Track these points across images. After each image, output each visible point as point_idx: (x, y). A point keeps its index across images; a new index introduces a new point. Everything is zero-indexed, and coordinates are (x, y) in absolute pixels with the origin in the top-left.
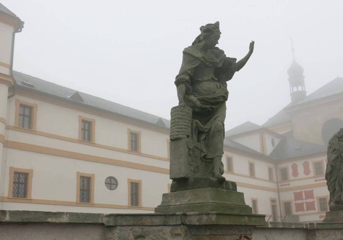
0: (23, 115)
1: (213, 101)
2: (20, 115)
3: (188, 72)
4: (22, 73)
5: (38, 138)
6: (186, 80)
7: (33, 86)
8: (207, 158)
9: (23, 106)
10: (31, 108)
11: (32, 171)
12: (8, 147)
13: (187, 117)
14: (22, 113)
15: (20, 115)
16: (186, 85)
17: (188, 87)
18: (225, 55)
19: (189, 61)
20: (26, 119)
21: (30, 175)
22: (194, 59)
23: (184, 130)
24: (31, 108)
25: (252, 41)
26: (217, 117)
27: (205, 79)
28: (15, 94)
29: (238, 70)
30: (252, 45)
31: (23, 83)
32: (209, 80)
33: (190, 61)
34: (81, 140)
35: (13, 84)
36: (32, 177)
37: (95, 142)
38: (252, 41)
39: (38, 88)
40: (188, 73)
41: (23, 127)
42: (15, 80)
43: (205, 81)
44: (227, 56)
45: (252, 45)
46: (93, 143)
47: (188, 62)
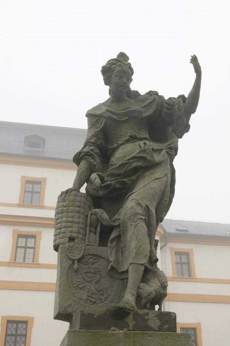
0: (181, 263)
1: (123, 171)
2: (177, 263)
3: (91, 141)
4: (184, 220)
5: (199, 285)
6: (84, 153)
7: (187, 231)
8: (120, 271)
9: (178, 253)
10: (187, 254)
11: (199, 324)
12: (170, 301)
13: (70, 208)
14: (179, 261)
15: (177, 263)
16: (88, 160)
17: (90, 162)
18: (182, 97)
19: (92, 124)
20: (185, 267)
21: (198, 330)
22: (98, 118)
23: (63, 230)
24: (187, 254)
25: (191, 56)
26: (131, 194)
27: (121, 142)
28: (167, 243)
29: (193, 111)
30: (194, 60)
31: (177, 230)
32: (128, 141)
33: (93, 124)
34: (176, 277)
35: (163, 233)
36: (201, 332)
37: (195, 276)
38: (191, 56)
39: (192, 231)
40: (91, 142)
41: (183, 275)
42: (164, 229)
43: (122, 144)
44: (166, 98)
45: (194, 60)
46: (194, 278)
47: (91, 127)
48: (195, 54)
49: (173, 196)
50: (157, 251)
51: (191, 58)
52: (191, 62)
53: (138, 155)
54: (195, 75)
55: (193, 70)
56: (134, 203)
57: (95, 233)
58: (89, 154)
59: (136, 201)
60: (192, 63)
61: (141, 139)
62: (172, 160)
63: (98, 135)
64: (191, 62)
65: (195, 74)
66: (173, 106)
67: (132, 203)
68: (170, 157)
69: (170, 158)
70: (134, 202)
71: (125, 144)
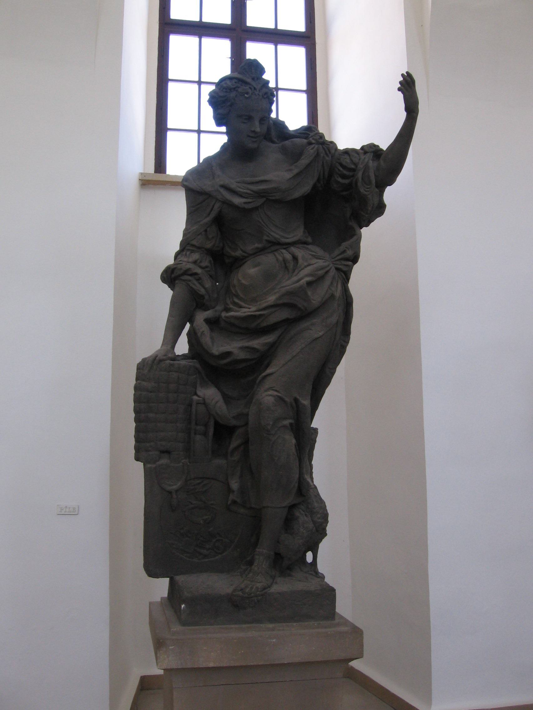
48: (411, 72)
49: (347, 342)
50: (313, 463)
51: (402, 79)
52: (399, 89)
53: (281, 302)
54: (403, 115)
55: (402, 105)
56: (270, 397)
57: (205, 434)
58: (190, 273)
59: (276, 393)
60: (403, 93)
61: (287, 246)
62: (346, 276)
63: (206, 231)
64: (399, 89)
65: (405, 114)
66: (354, 170)
67: (288, 236)
68: (344, 276)
69: (344, 279)
70: (271, 395)
71: (259, 255)
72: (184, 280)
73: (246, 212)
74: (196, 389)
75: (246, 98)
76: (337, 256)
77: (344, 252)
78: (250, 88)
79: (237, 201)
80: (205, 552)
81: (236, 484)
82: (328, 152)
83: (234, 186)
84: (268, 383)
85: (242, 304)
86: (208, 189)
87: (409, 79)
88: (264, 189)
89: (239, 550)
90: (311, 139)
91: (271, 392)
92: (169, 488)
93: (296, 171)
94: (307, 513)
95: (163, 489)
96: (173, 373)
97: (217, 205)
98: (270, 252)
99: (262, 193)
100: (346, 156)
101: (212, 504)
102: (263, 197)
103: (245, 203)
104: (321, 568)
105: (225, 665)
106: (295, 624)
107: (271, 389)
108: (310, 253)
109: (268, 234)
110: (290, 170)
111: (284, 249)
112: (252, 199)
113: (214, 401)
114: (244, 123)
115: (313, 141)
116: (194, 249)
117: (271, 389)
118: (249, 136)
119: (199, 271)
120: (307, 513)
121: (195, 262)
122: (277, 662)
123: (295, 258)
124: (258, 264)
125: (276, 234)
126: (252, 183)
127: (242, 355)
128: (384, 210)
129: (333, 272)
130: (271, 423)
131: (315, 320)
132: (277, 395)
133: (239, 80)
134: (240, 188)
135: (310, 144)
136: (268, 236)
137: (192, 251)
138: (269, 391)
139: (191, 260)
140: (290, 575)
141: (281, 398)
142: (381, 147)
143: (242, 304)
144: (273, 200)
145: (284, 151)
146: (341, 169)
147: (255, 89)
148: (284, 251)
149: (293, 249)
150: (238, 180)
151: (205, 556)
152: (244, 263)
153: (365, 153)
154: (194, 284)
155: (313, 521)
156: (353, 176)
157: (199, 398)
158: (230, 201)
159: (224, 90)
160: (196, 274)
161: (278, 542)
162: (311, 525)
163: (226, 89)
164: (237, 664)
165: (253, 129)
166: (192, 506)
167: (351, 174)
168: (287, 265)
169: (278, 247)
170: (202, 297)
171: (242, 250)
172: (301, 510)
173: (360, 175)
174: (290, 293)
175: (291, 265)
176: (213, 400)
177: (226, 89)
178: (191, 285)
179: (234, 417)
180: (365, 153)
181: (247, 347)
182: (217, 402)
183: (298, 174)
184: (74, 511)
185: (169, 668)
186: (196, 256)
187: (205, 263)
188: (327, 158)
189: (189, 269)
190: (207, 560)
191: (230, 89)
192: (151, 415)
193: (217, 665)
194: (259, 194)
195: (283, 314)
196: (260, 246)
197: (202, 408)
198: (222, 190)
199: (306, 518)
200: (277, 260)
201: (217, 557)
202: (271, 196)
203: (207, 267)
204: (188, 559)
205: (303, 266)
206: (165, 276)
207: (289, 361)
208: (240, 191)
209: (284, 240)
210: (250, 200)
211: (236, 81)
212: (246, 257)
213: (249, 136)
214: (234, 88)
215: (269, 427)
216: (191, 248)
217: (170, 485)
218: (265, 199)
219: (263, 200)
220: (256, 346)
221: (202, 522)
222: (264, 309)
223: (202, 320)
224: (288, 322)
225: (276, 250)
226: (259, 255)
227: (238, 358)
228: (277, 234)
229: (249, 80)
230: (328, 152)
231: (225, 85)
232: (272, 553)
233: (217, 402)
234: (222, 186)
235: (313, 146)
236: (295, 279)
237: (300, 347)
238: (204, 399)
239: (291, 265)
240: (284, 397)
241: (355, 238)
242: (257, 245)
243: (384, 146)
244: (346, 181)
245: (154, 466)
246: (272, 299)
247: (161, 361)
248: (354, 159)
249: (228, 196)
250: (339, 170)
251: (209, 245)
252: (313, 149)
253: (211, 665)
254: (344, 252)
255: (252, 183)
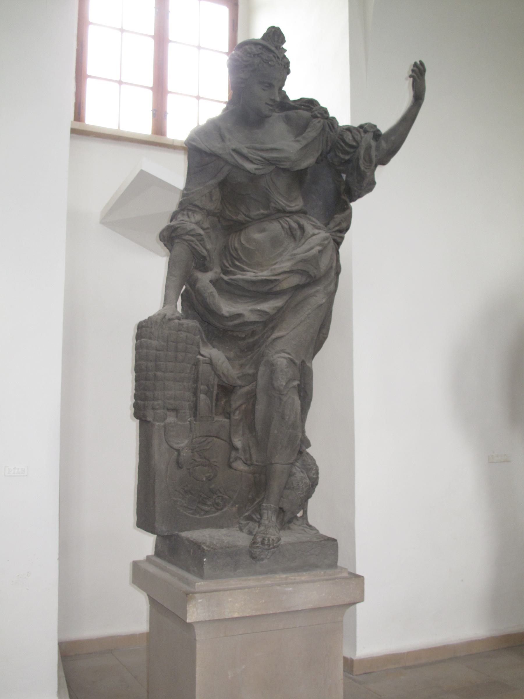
48: (424, 61)
53: (295, 268)
58: (192, 233)
61: (292, 213)
72: (186, 241)
73: (253, 177)
74: (199, 348)
75: (271, 66)
76: (334, 228)
77: (340, 224)
78: (274, 56)
79: (249, 166)
80: (206, 508)
81: (240, 442)
82: (332, 127)
83: (245, 151)
84: (279, 345)
85: (246, 268)
86: (220, 152)
87: (421, 67)
88: (277, 158)
89: (237, 506)
90: (316, 112)
91: (283, 355)
92: (176, 446)
93: (304, 143)
94: (303, 470)
95: (171, 447)
96: (182, 332)
97: (226, 169)
98: (274, 219)
99: (273, 161)
100: (348, 133)
101: (214, 462)
102: (272, 164)
103: (256, 169)
104: (311, 520)
105: (248, 615)
106: (304, 573)
107: (283, 351)
108: (311, 222)
109: (275, 202)
110: (298, 141)
111: (287, 217)
112: (263, 166)
113: (220, 361)
114: (264, 90)
115: (319, 115)
116: (197, 209)
117: (283, 351)
118: (267, 104)
119: (202, 232)
120: (303, 470)
121: (197, 223)
122: (292, 609)
123: (302, 228)
124: (263, 230)
125: (282, 202)
126: (262, 150)
127: (253, 318)
128: (374, 187)
129: (332, 241)
130: (284, 384)
131: (318, 288)
132: (289, 358)
133: (264, 46)
134: (251, 154)
135: (315, 117)
136: (275, 203)
137: (194, 212)
138: (281, 354)
139: (193, 220)
140: (289, 528)
141: (292, 360)
142: (379, 127)
143: (246, 268)
144: (282, 169)
145: (288, 120)
146: (344, 145)
147: (278, 58)
148: (288, 219)
149: (296, 217)
150: (248, 145)
151: (207, 512)
152: (248, 227)
153: (366, 132)
154: (197, 245)
155: (308, 476)
156: (355, 152)
157: (204, 358)
158: (242, 165)
159: (249, 55)
160: (200, 235)
161: (282, 497)
162: (308, 481)
163: (250, 54)
164: (259, 613)
165: (273, 98)
166: (197, 463)
167: (352, 150)
168: (294, 233)
169: (281, 215)
170: (204, 258)
171: (245, 215)
172: (296, 467)
173: (362, 152)
174: (304, 261)
175: (298, 233)
176: (219, 360)
177: (250, 54)
178: (194, 245)
179: (238, 378)
180: (366, 132)
181: (259, 311)
182: (223, 363)
183: (306, 146)
184: (23, 472)
185: (198, 621)
186: (198, 217)
187: (206, 225)
188: (331, 133)
189: (193, 230)
190: (208, 516)
191: (254, 55)
192: (159, 374)
193: (241, 615)
194: (269, 162)
195: (295, 280)
196: (265, 212)
197: (208, 368)
198: (233, 154)
199: (302, 474)
200: (282, 227)
201: (217, 514)
202: (283, 165)
203: (208, 228)
204: (191, 516)
205: (309, 236)
206: (165, 234)
207: (298, 325)
208: (251, 157)
209: (288, 209)
210: (261, 167)
211: (260, 47)
212: (248, 222)
213: (267, 104)
214: (258, 55)
215: (282, 388)
216: (193, 209)
217: (178, 443)
218: (274, 167)
219: (272, 168)
220: (267, 310)
221: (204, 479)
222: (279, 274)
223: (208, 281)
224: (298, 288)
225: (281, 218)
226: (263, 221)
227: (249, 320)
228: (282, 202)
229: (273, 48)
230: (332, 127)
231: (249, 50)
232: (278, 508)
233: (223, 363)
234: (234, 150)
235: (319, 119)
236: (306, 247)
237: (307, 313)
238: (211, 359)
239: (298, 233)
240: (294, 359)
241: (347, 212)
242: (262, 211)
243: (384, 128)
244: (347, 157)
245: (162, 424)
246: (286, 265)
247: (170, 320)
248: (356, 137)
249: (240, 161)
250: (341, 145)
251: (211, 206)
252: (319, 122)
253: (236, 615)
254: (340, 224)
255: (262, 150)
